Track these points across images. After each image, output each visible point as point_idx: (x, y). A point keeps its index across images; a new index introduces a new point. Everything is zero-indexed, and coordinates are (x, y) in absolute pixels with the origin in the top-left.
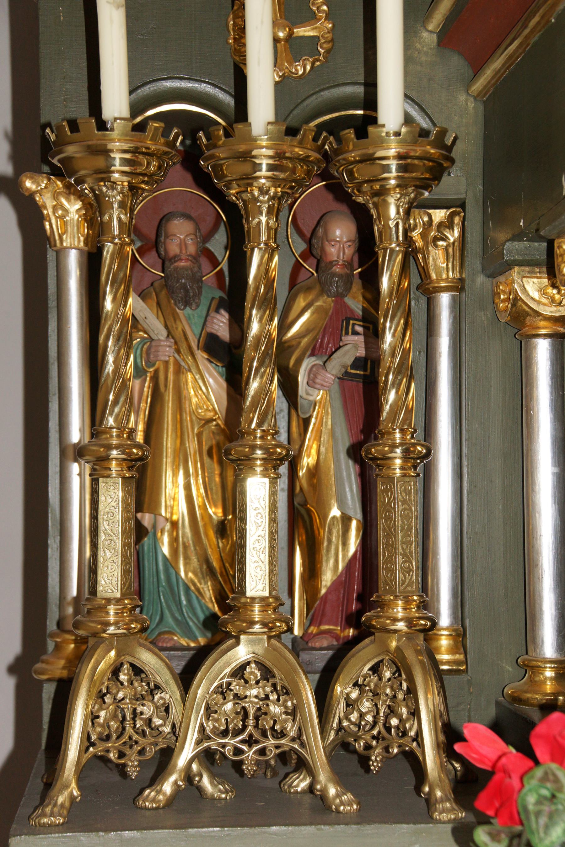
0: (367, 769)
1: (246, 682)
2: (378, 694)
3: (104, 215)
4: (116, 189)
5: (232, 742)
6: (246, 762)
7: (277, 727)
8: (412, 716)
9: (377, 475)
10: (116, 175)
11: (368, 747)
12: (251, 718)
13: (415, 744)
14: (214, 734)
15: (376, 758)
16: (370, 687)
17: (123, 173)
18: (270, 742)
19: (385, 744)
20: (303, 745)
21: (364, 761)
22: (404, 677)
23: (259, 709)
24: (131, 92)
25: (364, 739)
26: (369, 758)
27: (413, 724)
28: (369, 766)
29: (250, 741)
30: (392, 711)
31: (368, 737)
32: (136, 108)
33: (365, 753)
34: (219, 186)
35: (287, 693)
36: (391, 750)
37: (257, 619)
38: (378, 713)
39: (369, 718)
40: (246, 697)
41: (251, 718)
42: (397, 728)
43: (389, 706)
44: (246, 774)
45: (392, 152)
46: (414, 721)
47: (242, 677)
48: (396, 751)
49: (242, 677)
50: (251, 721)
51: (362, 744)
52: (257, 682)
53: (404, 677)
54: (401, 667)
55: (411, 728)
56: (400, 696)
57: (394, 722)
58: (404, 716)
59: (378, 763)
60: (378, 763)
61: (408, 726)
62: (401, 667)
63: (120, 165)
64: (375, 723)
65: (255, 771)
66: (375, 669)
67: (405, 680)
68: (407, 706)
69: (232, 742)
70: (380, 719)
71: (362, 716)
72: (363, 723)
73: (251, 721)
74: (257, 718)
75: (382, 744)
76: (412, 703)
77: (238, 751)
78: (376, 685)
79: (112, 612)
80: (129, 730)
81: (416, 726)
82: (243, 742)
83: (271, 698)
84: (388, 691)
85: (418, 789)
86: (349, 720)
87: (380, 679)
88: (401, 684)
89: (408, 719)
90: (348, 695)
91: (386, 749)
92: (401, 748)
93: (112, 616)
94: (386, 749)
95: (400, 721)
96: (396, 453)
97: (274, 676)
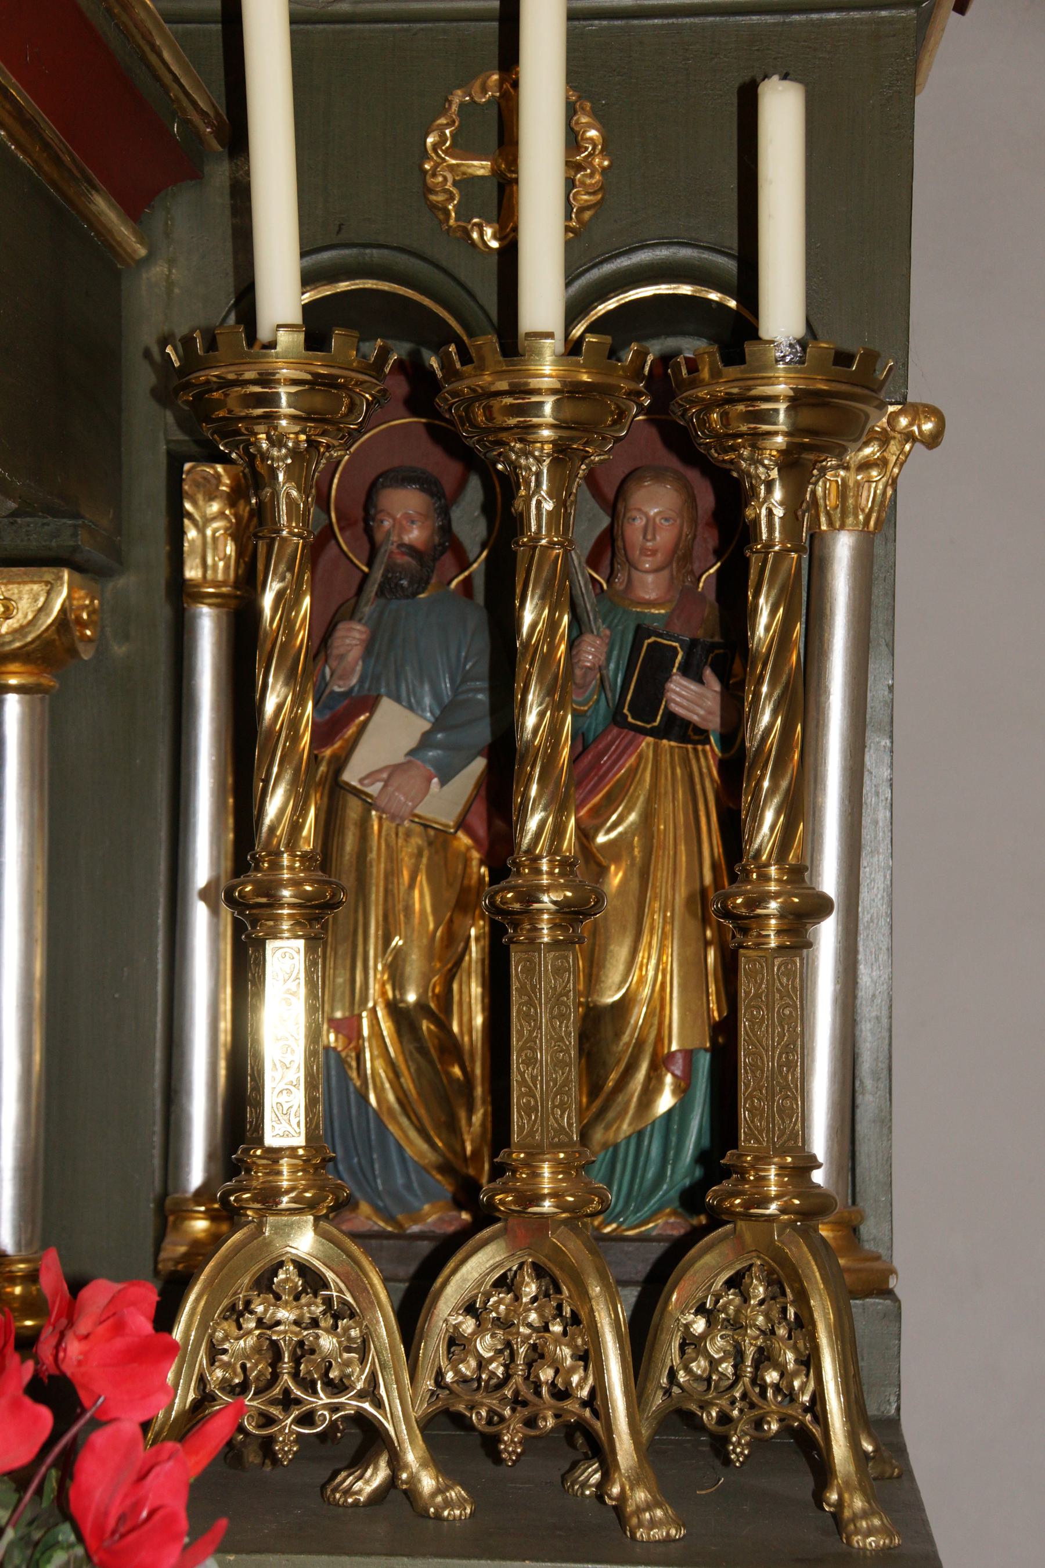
0: (496, 1458)
1: (278, 1297)
2: (742, 1327)
3: (263, 489)
4: (286, 446)
5: (254, 1403)
6: (506, 1438)
7: (559, 1381)
8: (803, 1368)
9: (511, 941)
10: (284, 423)
11: (724, 1419)
12: (286, 1360)
13: (808, 1417)
14: (222, 1389)
15: (511, 1439)
16: (727, 1314)
17: (293, 418)
18: (321, 1402)
19: (526, 1412)
20: (595, 1413)
21: (490, 1443)
22: (790, 1296)
23: (301, 1343)
24: (568, 284)
25: (716, 1405)
26: (727, 1440)
27: (807, 1381)
28: (727, 1454)
29: (287, 1401)
30: (765, 1358)
31: (723, 1402)
32: (574, 311)
33: (721, 1429)
34: (469, 443)
35: (352, 1315)
36: (766, 1427)
37: (546, 1191)
38: (513, 1356)
39: (727, 1368)
40: (278, 1323)
41: (286, 1360)
42: (777, 1388)
43: (534, 1347)
44: (505, 1460)
45: (782, 388)
46: (807, 1375)
47: (269, 1289)
48: (774, 1427)
49: (269, 1289)
50: (286, 1366)
51: (714, 1414)
52: (297, 1298)
53: (790, 1296)
54: (784, 1280)
55: (803, 1388)
56: (782, 1332)
57: (772, 1377)
58: (791, 1366)
59: (743, 1449)
60: (743, 1449)
61: (797, 1384)
62: (784, 1280)
63: (776, 411)
64: (738, 1376)
65: (519, 1455)
66: (735, 1282)
67: (793, 1303)
68: (795, 1349)
69: (254, 1403)
70: (745, 1371)
71: (714, 1363)
72: (484, 1376)
73: (286, 1366)
74: (297, 1361)
75: (523, 1412)
76: (805, 1345)
77: (268, 1421)
78: (738, 1311)
79: (285, 1170)
80: (518, 1380)
81: (812, 1385)
82: (273, 1402)
83: (322, 1324)
84: (533, 1317)
85: (819, 1498)
86: (688, 1371)
87: (517, 1298)
88: (784, 1310)
89: (795, 1374)
90: (687, 1326)
91: (530, 1422)
92: (561, 1420)
93: (546, 1180)
94: (530, 1422)
95: (782, 1376)
96: (542, 902)
97: (326, 1286)
